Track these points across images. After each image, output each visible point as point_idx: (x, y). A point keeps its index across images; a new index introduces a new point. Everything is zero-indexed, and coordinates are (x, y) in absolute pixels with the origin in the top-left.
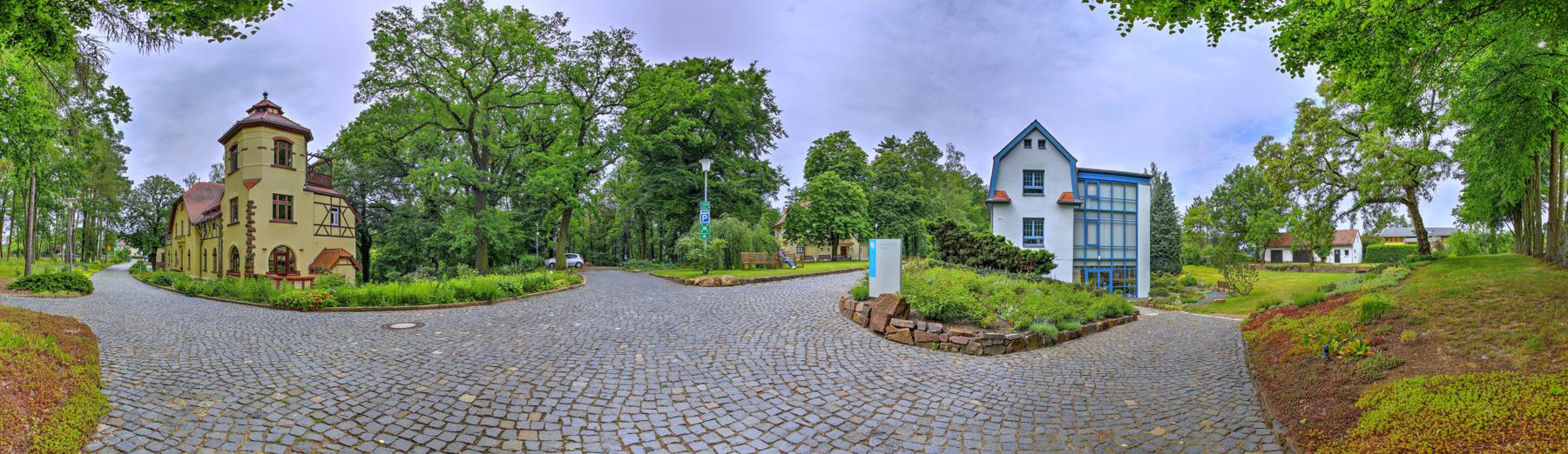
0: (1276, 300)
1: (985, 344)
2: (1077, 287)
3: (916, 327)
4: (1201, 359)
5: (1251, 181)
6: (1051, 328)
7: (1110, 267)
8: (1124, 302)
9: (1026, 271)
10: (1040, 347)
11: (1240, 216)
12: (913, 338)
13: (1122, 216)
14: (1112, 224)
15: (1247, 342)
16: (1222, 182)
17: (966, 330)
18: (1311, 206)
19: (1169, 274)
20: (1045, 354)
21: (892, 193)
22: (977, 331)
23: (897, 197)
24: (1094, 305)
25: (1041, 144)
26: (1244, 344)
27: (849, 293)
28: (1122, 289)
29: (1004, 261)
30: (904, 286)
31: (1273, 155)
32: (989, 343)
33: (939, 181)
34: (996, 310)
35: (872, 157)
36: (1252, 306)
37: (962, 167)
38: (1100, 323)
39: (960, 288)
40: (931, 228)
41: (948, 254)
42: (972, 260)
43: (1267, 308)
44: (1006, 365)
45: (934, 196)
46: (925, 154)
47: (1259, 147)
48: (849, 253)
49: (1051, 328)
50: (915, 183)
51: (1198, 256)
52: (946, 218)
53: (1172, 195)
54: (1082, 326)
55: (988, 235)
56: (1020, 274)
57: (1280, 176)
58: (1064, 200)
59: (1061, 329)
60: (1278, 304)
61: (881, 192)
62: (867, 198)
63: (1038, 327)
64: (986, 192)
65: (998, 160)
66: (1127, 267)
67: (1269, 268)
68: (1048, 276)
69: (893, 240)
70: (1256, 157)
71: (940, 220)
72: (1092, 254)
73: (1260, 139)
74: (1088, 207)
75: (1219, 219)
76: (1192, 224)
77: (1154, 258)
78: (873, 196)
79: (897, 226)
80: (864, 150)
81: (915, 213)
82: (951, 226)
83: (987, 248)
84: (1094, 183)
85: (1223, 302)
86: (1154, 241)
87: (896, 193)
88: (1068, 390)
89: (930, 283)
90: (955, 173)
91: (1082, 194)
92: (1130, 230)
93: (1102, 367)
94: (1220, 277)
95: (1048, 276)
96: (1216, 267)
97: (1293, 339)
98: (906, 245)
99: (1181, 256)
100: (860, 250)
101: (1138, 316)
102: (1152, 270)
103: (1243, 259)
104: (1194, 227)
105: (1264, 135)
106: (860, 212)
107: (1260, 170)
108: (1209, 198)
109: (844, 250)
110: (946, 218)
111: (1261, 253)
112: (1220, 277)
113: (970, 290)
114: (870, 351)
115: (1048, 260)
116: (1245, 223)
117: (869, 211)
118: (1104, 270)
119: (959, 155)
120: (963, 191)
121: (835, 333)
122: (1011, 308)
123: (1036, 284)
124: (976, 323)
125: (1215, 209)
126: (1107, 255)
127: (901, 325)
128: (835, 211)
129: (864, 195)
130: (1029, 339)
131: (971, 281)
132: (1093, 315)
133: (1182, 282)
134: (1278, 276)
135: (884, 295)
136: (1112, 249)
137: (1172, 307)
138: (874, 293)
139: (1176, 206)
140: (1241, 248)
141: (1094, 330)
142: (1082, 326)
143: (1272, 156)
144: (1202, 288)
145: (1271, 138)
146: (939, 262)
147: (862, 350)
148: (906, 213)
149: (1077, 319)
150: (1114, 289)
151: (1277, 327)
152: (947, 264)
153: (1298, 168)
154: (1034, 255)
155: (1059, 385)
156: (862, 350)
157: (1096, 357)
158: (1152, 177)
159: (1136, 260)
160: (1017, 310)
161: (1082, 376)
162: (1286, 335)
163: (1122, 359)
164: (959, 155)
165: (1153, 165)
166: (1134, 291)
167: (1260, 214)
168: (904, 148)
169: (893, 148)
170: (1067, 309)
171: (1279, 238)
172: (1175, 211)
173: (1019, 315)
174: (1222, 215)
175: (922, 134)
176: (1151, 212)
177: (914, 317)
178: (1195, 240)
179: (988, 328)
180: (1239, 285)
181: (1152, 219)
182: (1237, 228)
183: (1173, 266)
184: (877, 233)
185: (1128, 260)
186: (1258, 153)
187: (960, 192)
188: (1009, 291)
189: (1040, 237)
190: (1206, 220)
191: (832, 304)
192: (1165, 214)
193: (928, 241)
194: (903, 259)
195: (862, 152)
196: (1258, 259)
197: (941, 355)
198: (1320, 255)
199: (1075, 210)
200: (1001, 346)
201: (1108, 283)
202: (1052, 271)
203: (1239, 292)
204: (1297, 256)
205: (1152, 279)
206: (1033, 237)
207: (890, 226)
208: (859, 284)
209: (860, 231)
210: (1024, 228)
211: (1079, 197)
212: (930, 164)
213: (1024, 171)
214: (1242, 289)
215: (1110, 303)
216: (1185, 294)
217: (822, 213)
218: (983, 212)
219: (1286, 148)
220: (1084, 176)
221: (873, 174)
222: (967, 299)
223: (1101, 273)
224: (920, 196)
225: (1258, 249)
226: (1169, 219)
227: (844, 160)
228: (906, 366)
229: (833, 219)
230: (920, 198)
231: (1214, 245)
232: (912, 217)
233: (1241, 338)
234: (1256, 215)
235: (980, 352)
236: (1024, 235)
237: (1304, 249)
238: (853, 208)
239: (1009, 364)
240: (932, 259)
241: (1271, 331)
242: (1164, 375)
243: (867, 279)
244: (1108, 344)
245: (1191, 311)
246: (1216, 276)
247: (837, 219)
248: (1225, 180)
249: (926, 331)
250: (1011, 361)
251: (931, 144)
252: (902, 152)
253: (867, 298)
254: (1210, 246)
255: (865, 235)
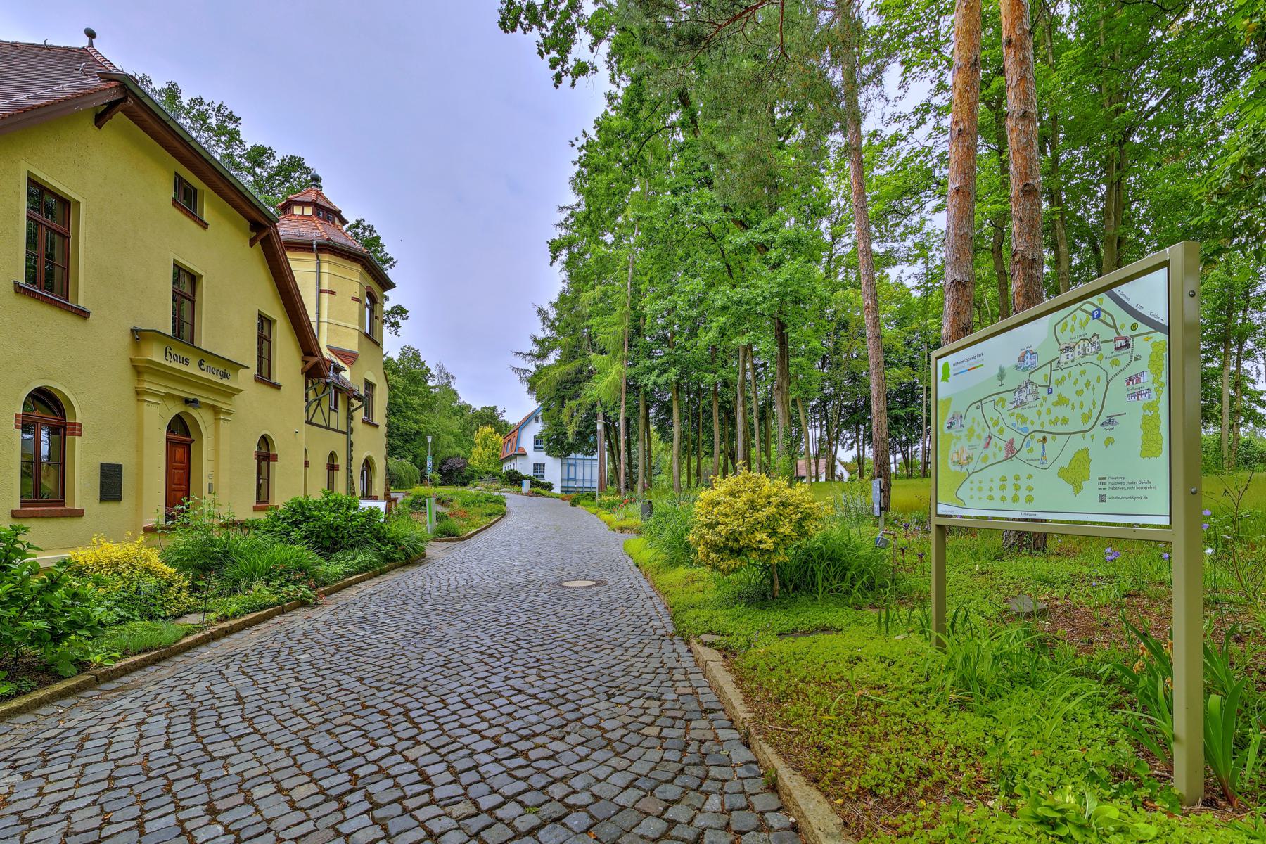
72: (571, 484)
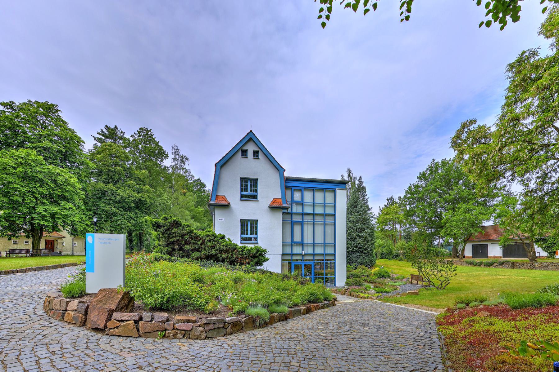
0: (478, 296)
1: (207, 328)
2: (285, 277)
3: (141, 319)
4: (393, 348)
5: (448, 175)
6: (263, 312)
7: (312, 260)
8: (324, 289)
9: (242, 264)
10: (254, 328)
11: (435, 212)
12: (138, 330)
13: (322, 218)
14: (314, 224)
15: (443, 337)
16: (415, 181)
17: (191, 317)
18: (530, 191)
19: (363, 266)
20: (259, 334)
21: (114, 188)
22: (200, 316)
23: (120, 192)
24: (299, 292)
25: (256, 154)
26: (440, 340)
27: (59, 290)
28: (323, 279)
29: (224, 256)
30: (127, 279)
31: (476, 141)
32: (211, 327)
33: (165, 182)
34: (217, 298)
35: (89, 145)
36: (450, 301)
37: (186, 171)
38: (304, 307)
39: (185, 279)
40: (157, 226)
41: (173, 249)
42: (196, 254)
43: (467, 305)
44: (226, 346)
45: (159, 196)
46: (150, 153)
47: (458, 136)
48: (58, 247)
49: (263, 312)
50: (139, 180)
51: (391, 251)
52: (171, 217)
53: (367, 197)
54: (289, 309)
55: (210, 233)
56: (237, 266)
57: (485, 164)
58: (275, 205)
59: (271, 313)
60: (482, 301)
61: (101, 185)
62: (83, 189)
63: (253, 311)
64: (208, 195)
65: (219, 167)
66: (327, 260)
67: (471, 263)
68: (262, 267)
69: (115, 236)
70: (454, 148)
71: (166, 218)
72: (297, 250)
73: (458, 127)
74: (295, 210)
75: (412, 216)
76: (385, 222)
77: (350, 253)
78: (90, 188)
79: (119, 222)
80: (78, 134)
81: (140, 210)
82: (177, 224)
83: (210, 244)
84: (299, 189)
85: (416, 294)
86: (350, 238)
87: (119, 188)
88: (277, 368)
89: (156, 276)
90: (180, 176)
91: (289, 199)
92: (329, 230)
93: (306, 346)
94: (414, 270)
95: (262, 267)
96: (409, 260)
97: (503, 343)
98: (131, 241)
99: (375, 251)
100: (74, 244)
101: (336, 302)
102: (348, 263)
103: (439, 254)
104: (387, 225)
105: (464, 119)
106: (74, 204)
107: (459, 162)
108: (402, 197)
109: (50, 244)
110: (171, 217)
111: (459, 248)
112: (414, 270)
113: (195, 281)
114: (88, 352)
115: (261, 254)
116: (441, 219)
117: (85, 203)
118: (307, 263)
119: (184, 159)
120: (188, 194)
121: (36, 340)
122: (231, 295)
123: (251, 274)
124: (199, 310)
125: (408, 207)
126: (309, 250)
127: (124, 318)
128: (36, 199)
129: (79, 186)
130: (246, 322)
131: (195, 273)
132: (298, 300)
133: (375, 274)
134: (483, 272)
135: (105, 290)
136: (314, 245)
137: (367, 295)
138: (92, 286)
139: (370, 207)
140: (436, 243)
141: (299, 313)
142: (289, 309)
143: (473, 143)
144: (395, 280)
145: (473, 122)
146: (164, 256)
147: (76, 353)
148: (130, 209)
149: (285, 303)
150: (316, 279)
151: (480, 326)
152: (173, 258)
153: (510, 150)
154: (249, 251)
155: (271, 363)
156: (76, 353)
157: (301, 338)
158: (348, 182)
159: (334, 255)
160: (235, 297)
161: (289, 354)
162: (496, 337)
163: (321, 340)
164: (184, 159)
165: (349, 171)
166: (332, 281)
167: (459, 208)
168: (128, 144)
169: (115, 140)
170: (277, 295)
171: (483, 232)
172: (369, 212)
173: (238, 300)
174: (415, 213)
175: (147, 131)
176: (348, 213)
177: (139, 308)
178: (388, 236)
179: (211, 313)
180: (433, 279)
181: (348, 220)
182: (431, 224)
183: (367, 260)
184: (95, 227)
185: (294, 254)
186: (456, 143)
187: (185, 194)
188: (228, 281)
189: (255, 236)
190: (398, 218)
191: (32, 306)
192: (359, 215)
193: (153, 237)
194: (127, 253)
195: (76, 136)
196: (457, 254)
197: (166, 342)
198: (545, 249)
199: (283, 213)
200: (221, 329)
201: (311, 273)
202: (265, 264)
203: (434, 286)
204: (508, 251)
205: (348, 271)
206: (249, 235)
207: (111, 222)
208: (73, 280)
209: (73, 224)
210: (241, 228)
211: (287, 202)
212: (155, 164)
213: (242, 179)
214: (437, 283)
215: (312, 290)
216: (378, 285)
217: (15, 198)
218: (206, 212)
219: (493, 129)
220: (290, 184)
221: (90, 163)
222: (191, 289)
223: (305, 265)
224: (146, 195)
225: (456, 244)
226: (364, 219)
227: (51, 141)
228: (130, 360)
229: (34, 208)
230: (145, 196)
231: (407, 241)
232: (136, 214)
233: (435, 333)
234: (453, 209)
235: (203, 336)
236: (241, 233)
237: (520, 242)
238: (65, 198)
239: (229, 345)
240: (158, 254)
241: (473, 329)
242: (359, 358)
243: (83, 274)
244: (310, 326)
245: (384, 301)
246: (410, 269)
247: (40, 209)
248: (418, 178)
249: (151, 321)
250: (231, 342)
251: (157, 144)
252: (126, 147)
253: (82, 294)
254: (403, 242)
255: (80, 229)
